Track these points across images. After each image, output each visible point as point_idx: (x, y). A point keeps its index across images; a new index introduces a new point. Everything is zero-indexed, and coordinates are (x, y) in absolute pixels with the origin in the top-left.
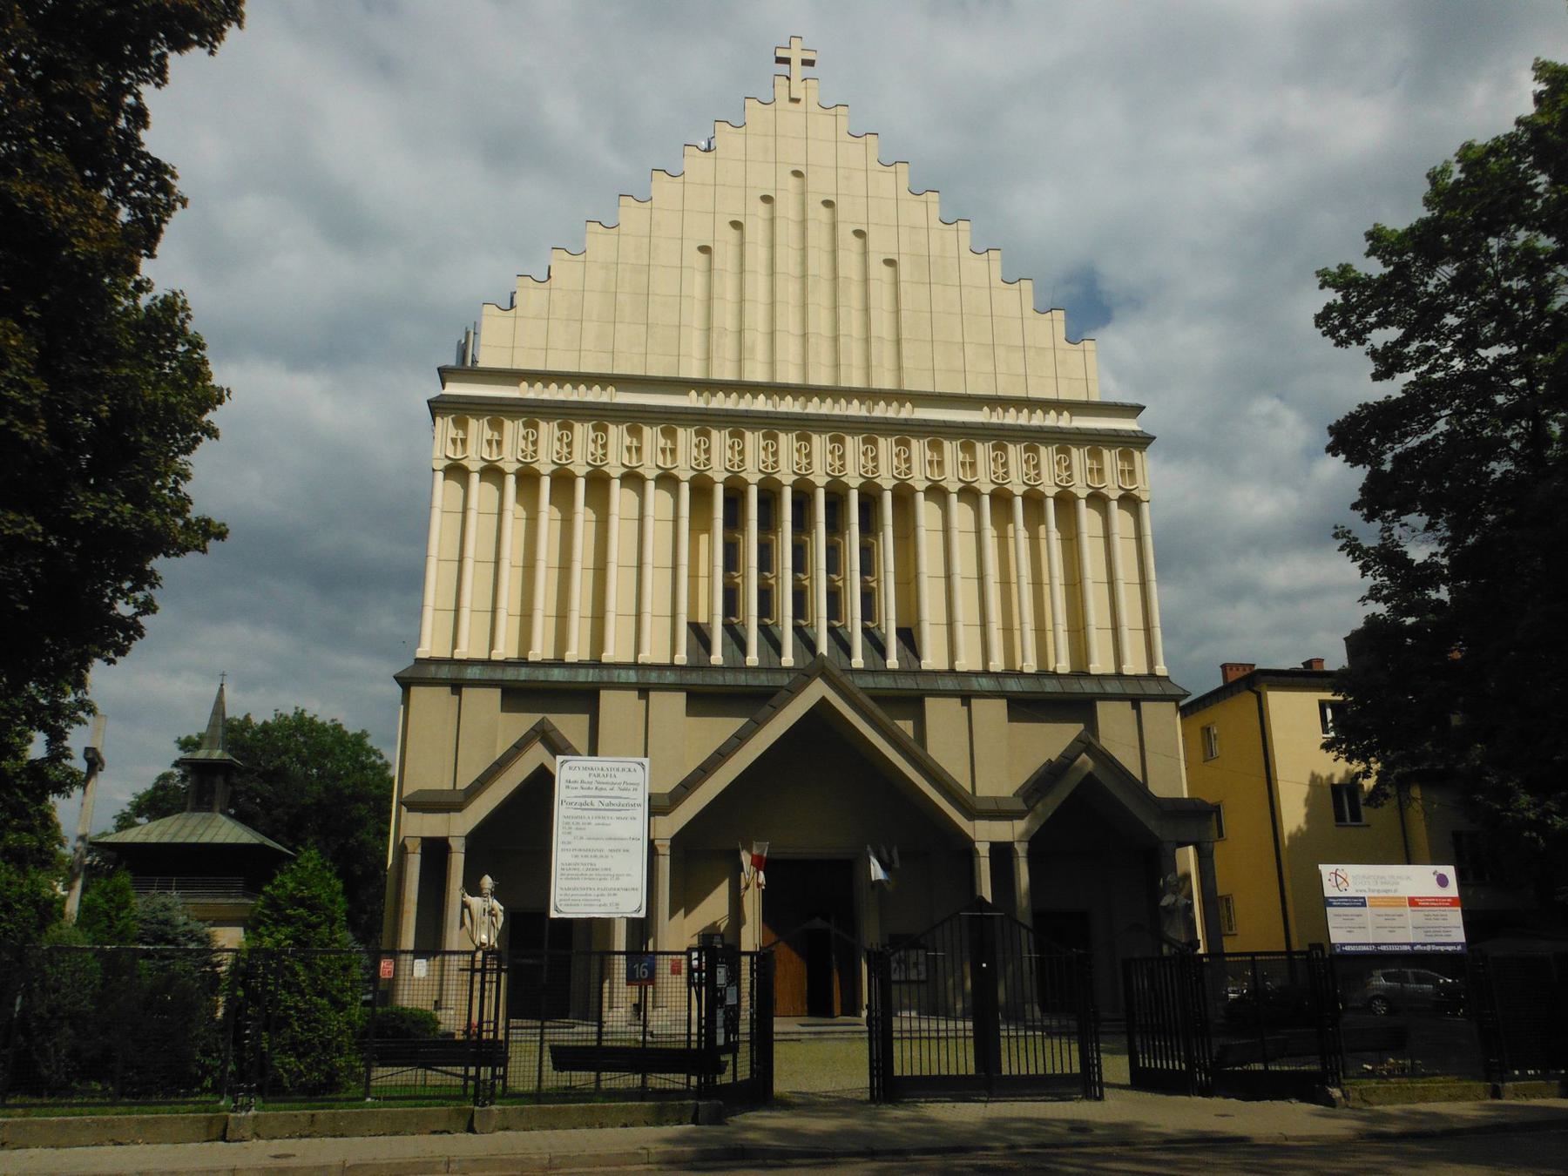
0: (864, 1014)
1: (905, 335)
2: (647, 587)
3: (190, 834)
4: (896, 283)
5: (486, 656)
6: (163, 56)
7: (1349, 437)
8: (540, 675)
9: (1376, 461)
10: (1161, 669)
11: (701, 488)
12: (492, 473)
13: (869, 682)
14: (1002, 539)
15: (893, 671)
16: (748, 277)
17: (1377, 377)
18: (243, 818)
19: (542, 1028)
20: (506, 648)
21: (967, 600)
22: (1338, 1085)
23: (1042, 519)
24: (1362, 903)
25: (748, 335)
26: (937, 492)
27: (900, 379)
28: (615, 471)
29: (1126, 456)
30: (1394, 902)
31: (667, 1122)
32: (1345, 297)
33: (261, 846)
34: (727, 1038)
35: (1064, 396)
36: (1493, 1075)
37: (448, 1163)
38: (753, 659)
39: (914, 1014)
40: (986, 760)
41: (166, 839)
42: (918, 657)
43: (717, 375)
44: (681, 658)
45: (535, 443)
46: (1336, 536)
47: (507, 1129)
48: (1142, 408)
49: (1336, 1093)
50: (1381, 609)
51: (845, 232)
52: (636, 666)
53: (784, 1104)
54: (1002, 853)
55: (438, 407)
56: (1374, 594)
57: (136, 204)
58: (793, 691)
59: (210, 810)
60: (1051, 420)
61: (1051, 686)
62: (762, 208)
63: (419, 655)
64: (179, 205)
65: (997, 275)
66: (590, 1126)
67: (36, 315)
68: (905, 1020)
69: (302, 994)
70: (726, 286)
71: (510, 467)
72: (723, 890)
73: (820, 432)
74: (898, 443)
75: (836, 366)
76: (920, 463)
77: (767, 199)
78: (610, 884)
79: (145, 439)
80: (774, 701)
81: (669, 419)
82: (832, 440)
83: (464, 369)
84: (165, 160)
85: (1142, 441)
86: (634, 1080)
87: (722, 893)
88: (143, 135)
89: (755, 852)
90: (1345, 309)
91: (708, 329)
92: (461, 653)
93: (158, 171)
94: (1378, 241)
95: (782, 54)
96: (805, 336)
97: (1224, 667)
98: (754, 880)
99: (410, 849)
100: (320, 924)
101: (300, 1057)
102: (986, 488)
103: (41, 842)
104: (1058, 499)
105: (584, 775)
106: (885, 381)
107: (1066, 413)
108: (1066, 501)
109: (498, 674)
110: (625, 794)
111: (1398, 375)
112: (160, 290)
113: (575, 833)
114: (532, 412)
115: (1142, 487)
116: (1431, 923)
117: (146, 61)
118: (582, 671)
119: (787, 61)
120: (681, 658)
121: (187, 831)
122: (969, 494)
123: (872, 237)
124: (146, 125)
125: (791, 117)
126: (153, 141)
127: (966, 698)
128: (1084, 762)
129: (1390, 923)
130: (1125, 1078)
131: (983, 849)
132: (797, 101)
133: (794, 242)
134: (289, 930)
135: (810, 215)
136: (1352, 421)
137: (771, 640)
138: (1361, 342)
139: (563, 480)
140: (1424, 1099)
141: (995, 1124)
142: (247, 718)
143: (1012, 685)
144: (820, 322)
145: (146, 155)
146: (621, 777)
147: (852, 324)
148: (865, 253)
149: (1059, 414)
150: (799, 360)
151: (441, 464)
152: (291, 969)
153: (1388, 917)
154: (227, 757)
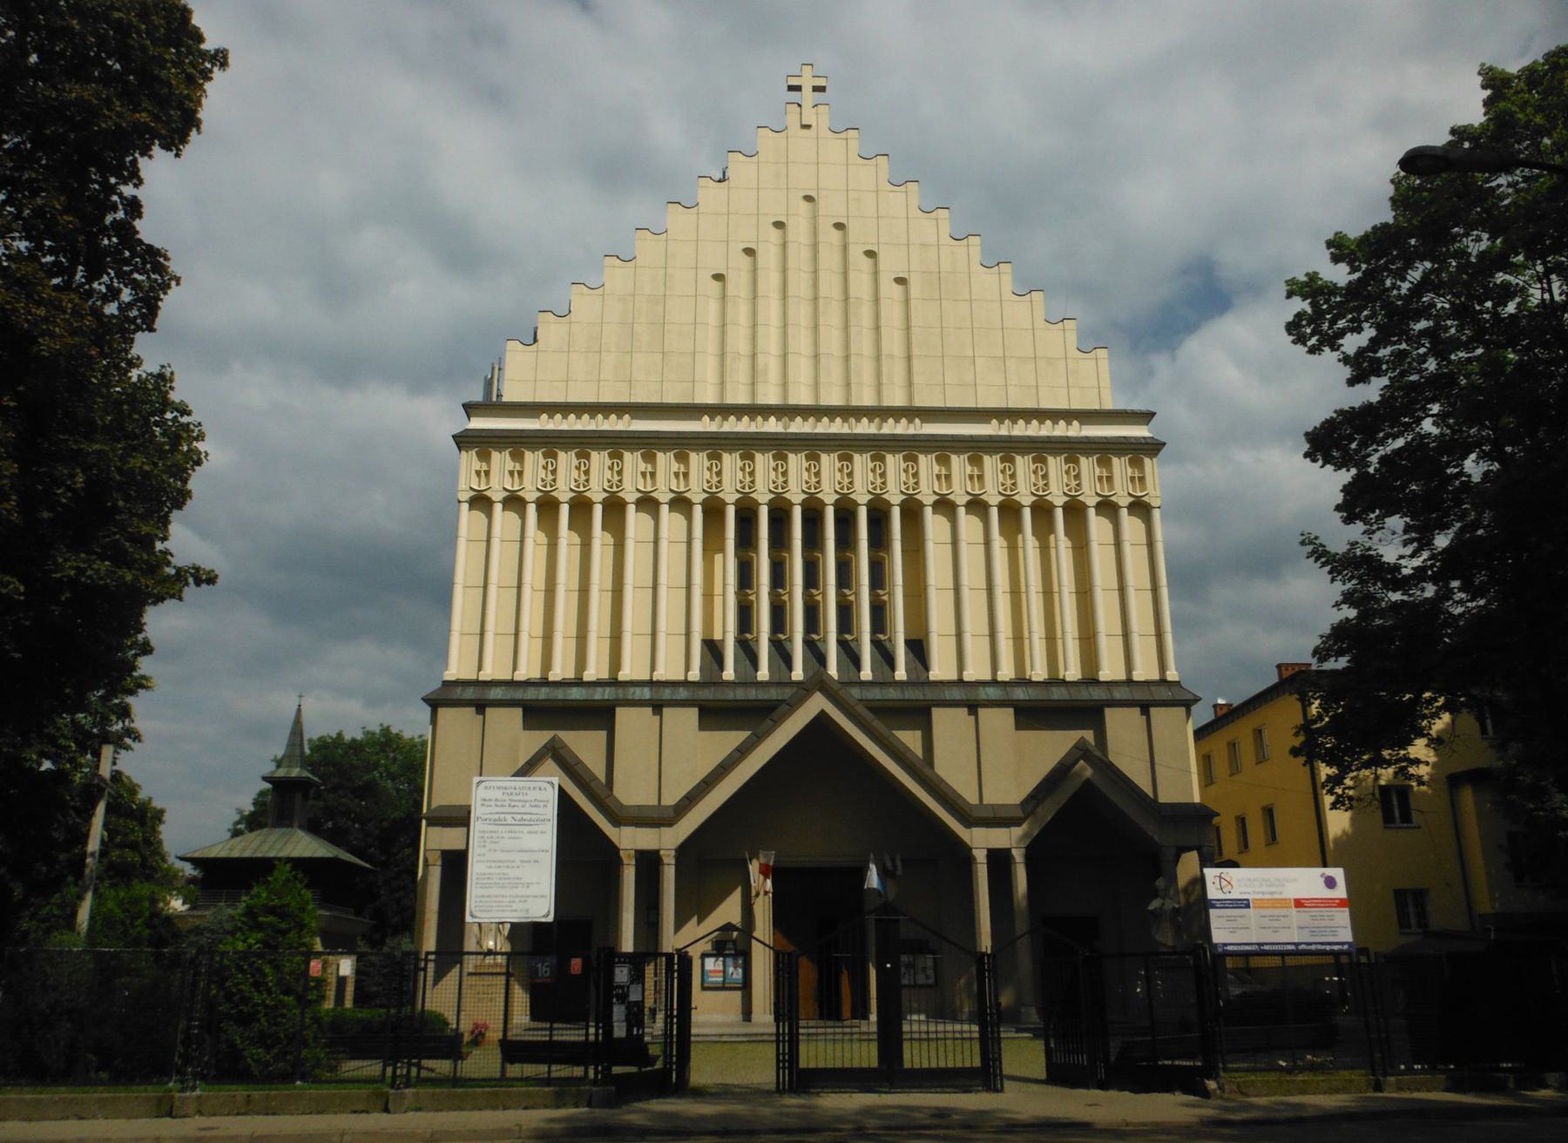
0: (873, 1017)
1: (915, 351)
2: (662, 606)
3: (271, 849)
4: (907, 301)
5: (509, 677)
6: (135, 162)
7: (1326, 443)
8: (559, 694)
9: (1362, 463)
10: (1172, 675)
11: (713, 510)
12: (514, 502)
13: (876, 694)
14: (1013, 550)
15: (901, 683)
16: (761, 303)
17: (1351, 382)
18: (313, 828)
19: (551, 1029)
20: (528, 669)
21: (977, 610)
22: (1215, 1079)
23: (1051, 529)
24: (1245, 904)
25: (761, 359)
26: (945, 506)
27: (910, 396)
28: (630, 496)
29: (1136, 463)
30: (1282, 903)
31: (565, 1105)
32: (1314, 305)
33: (334, 861)
34: (629, 1030)
35: (1076, 406)
36: (1379, 1068)
37: (342, 1135)
38: (763, 674)
39: (923, 1017)
40: (989, 770)
41: (247, 854)
42: (927, 669)
43: (730, 399)
44: (695, 675)
45: (554, 472)
46: (1303, 543)
47: (419, 1109)
48: (1154, 414)
49: (1212, 1085)
50: (1352, 613)
51: (856, 252)
52: (651, 683)
53: (699, 1093)
54: (1000, 860)
55: (464, 440)
56: (1348, 598)
57: (136, 285)
58: (792, 705)
59: (290, 826)
60: (1060, 430)
61: (1058, 694)
62: (775, 234)
63: (447, 678)
64: (173, 283)
65: (1008, 288)
66: (494, 1108)
67: (12, 404)
68: (915, 1023)
69: (270, 992)
70: (740, 313)
71: (531, 495)
72: (737, 896)
73: (828, 451)
74: (906, 459)
75: (848, 385)
76: (928, 477)
77: (779, 225)
78: (520, 891)
79: (121, 503)
80: (774, 715)
81: (682, 444)
82: (841, 458)
83: (491, 405)
84: (157, 245)
85: (1153, 447)
86: (542, 1069)
87: (735, 898)
88: (137, 223)
89: (762, 860)
90: (1316, 317)
91: (722, 355)
92: (487, 674)
93: (153, 258)
94: (1339, 249)
95: (794, 82)
96: (816, 357)
97: (1279, 666)
98: (762, 885)
99: (666, 860)
100: (289, 930)
101: (268, 1049)
102: (994, 499)
103: (144, 858)
104: (1067, 508)
105: (498, 794)
106: (896, 399)
107: (1075, 423)
108: (1075, 510)
109: (519, 694)
110: (534, 810)
111: (1373, 379)
112: (150, 366)
113: (489, 846)
114: (550, 443)
115: (1152, 493)
116: (1316, 923)
117: (122, 166)
118: (600, 689)
119: (798, 88)
120: (695, 675)
121: (266, 847)
122: (977, 506)
123: (881, 257)
124: (140, 216)
125: (802, 144)
126: (147, 230)
127: (973, 707)
128: (1083, 769)
129: (1275, 924)
130: (1039, 1069)
131: (980, 856)
132: (808, 127)
133: (806, 267)
134: (260, 935)
135: (821, 238)
136: (1329, 425)
137: (781, 652)
138: (1335, 347)
139: (581, 506)
140: (1303, 1092)
141: (868, 1112)
142: (340, 735)
143: (1020, 694)
144: (832, 341)
145: (140, 242)
146: (532, 795)
147: (863, 344)
148: (876, 273)
149: (1069, 423)
150: (811, 382)
151: (465, 496)
152: (260, 970)
153: (1273, 918)
154: (306, 774)
